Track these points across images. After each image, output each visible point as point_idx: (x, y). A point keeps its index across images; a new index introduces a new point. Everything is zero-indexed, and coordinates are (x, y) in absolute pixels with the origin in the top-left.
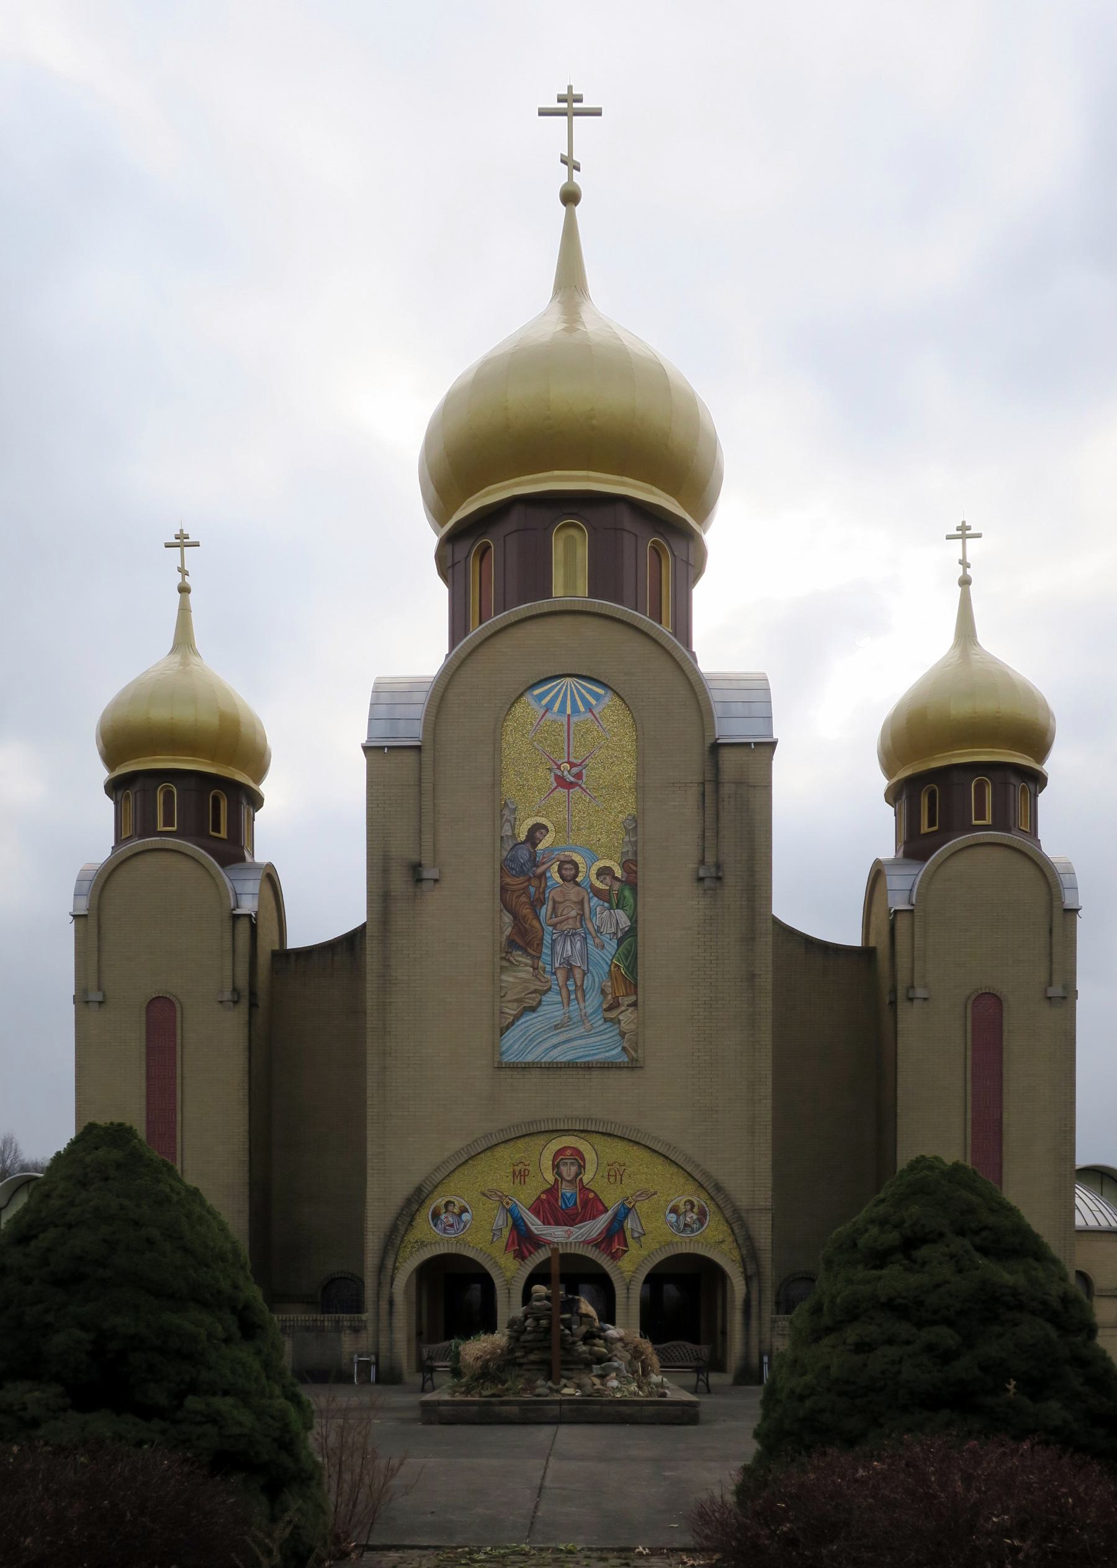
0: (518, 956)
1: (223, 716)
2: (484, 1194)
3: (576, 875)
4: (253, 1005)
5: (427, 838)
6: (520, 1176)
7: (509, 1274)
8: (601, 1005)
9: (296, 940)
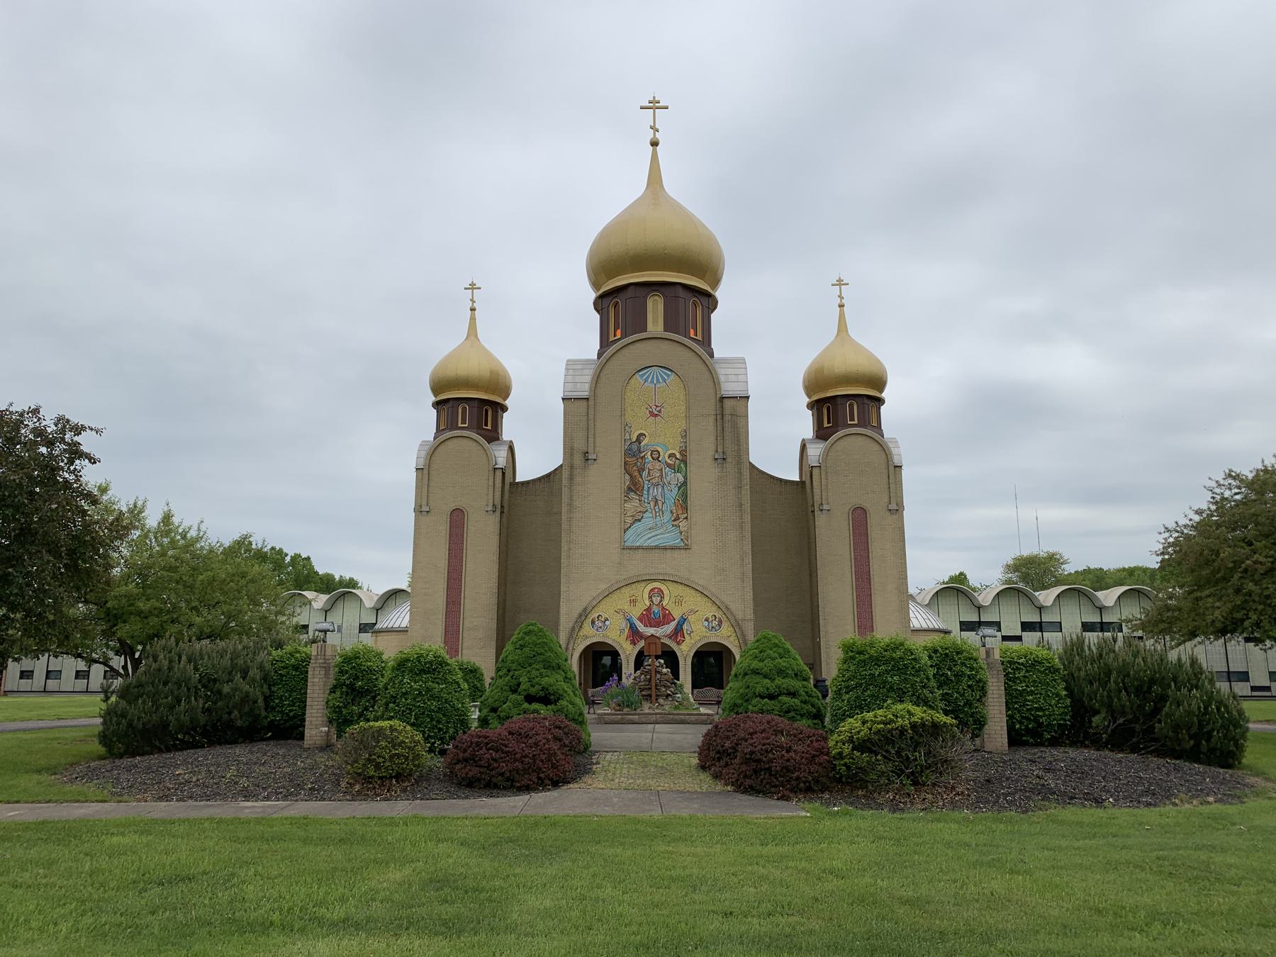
0: (632, 495)
1: (491, 372)
2: (615, 611)
3: (659, 457)
4: (502, 512)
5: (591, 440)
6: (633, 602)
7: (628, 652)
8: (670, 519)
9: (520, 478)
